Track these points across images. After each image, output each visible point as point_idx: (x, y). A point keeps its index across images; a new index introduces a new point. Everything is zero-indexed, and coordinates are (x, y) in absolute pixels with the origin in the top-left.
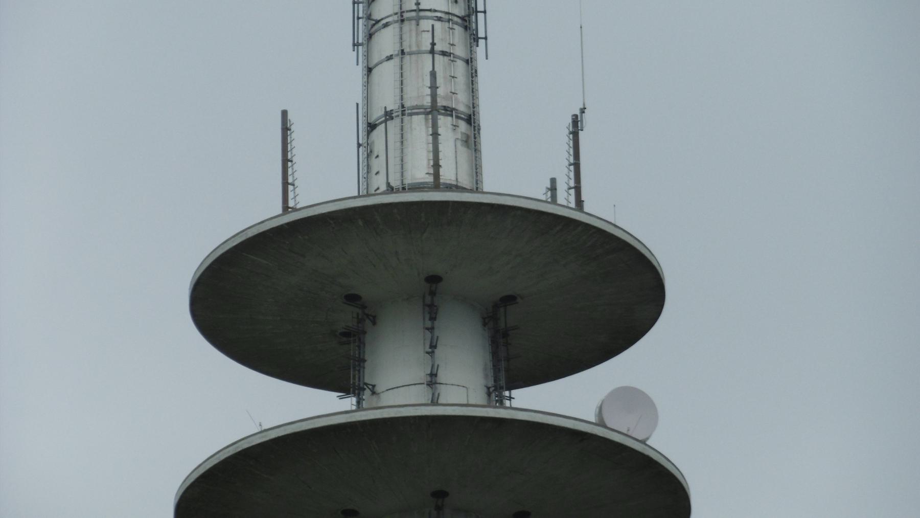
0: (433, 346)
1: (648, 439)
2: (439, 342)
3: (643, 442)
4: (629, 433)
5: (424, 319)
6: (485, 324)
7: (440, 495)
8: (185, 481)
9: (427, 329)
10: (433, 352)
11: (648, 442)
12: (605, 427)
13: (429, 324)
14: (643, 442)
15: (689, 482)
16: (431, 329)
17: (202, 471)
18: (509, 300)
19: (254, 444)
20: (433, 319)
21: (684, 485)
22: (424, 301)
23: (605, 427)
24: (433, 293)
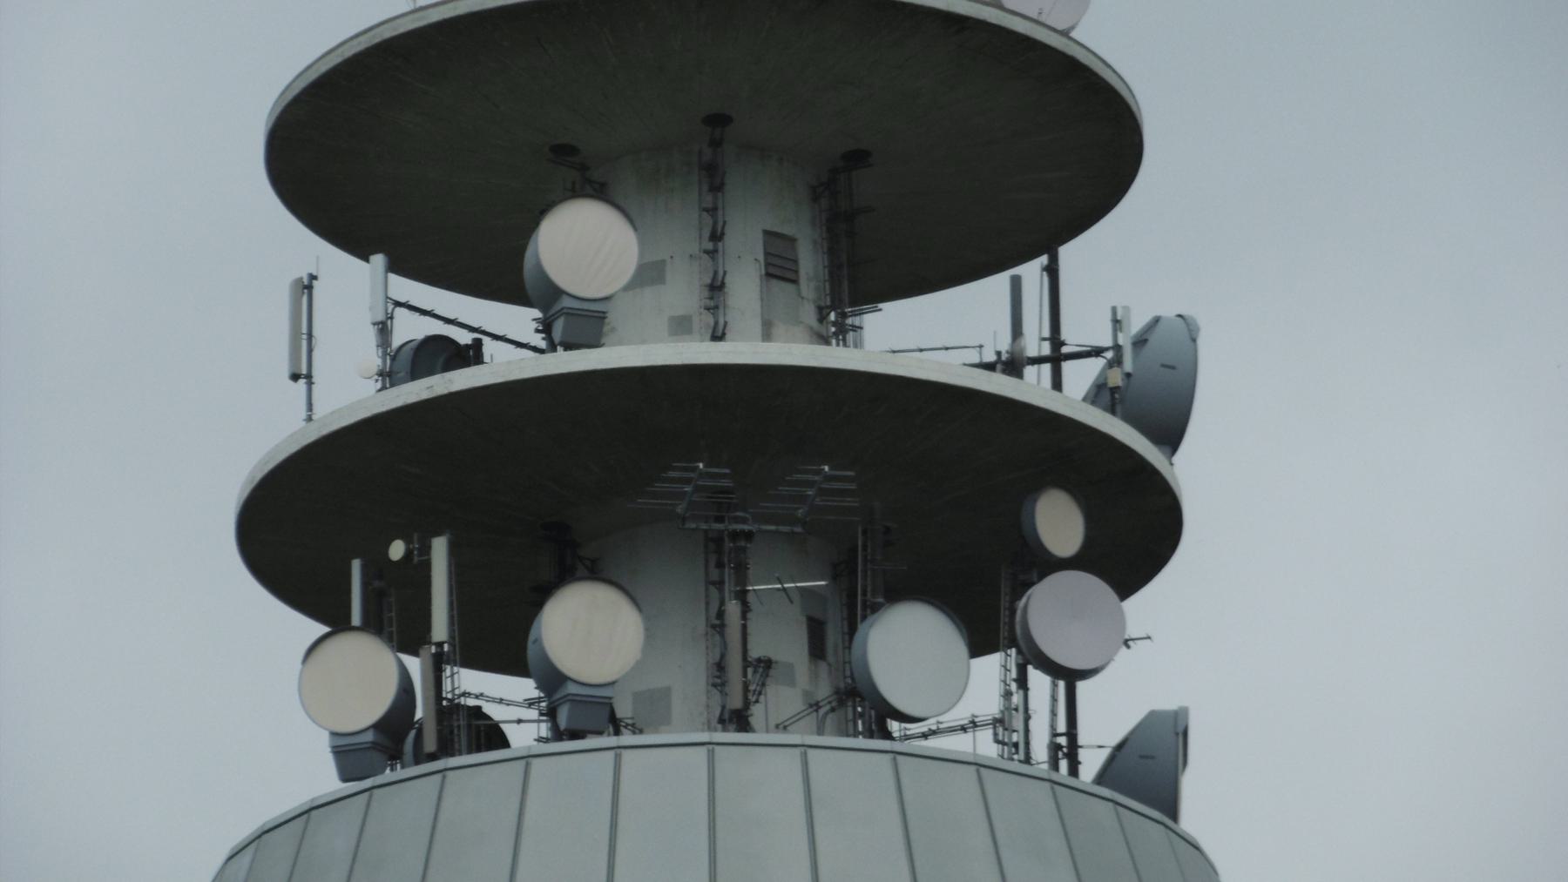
0: (717, 236)
1: (1073, 28)
2: (727, 231)
3: (1065, 34)
4: (1043, 19)
5: (707, 561)
6: (815, 198)
7: (718, 120)
8: (283, 93)
9: (707, 210)
10: (715, 251)
11: (1074, 34)
12: (1002, 8)
13: (708, 200)
14: (1065, 34)
15: (1138, 97)
16: (712, 211)
17: (313, 75)
18: (857, 158)
19: (402, 30)
20: (717, 188)
21: (1134, 109)
22: (707, 574)
23: (1002, 8)
24: (716, 144)
